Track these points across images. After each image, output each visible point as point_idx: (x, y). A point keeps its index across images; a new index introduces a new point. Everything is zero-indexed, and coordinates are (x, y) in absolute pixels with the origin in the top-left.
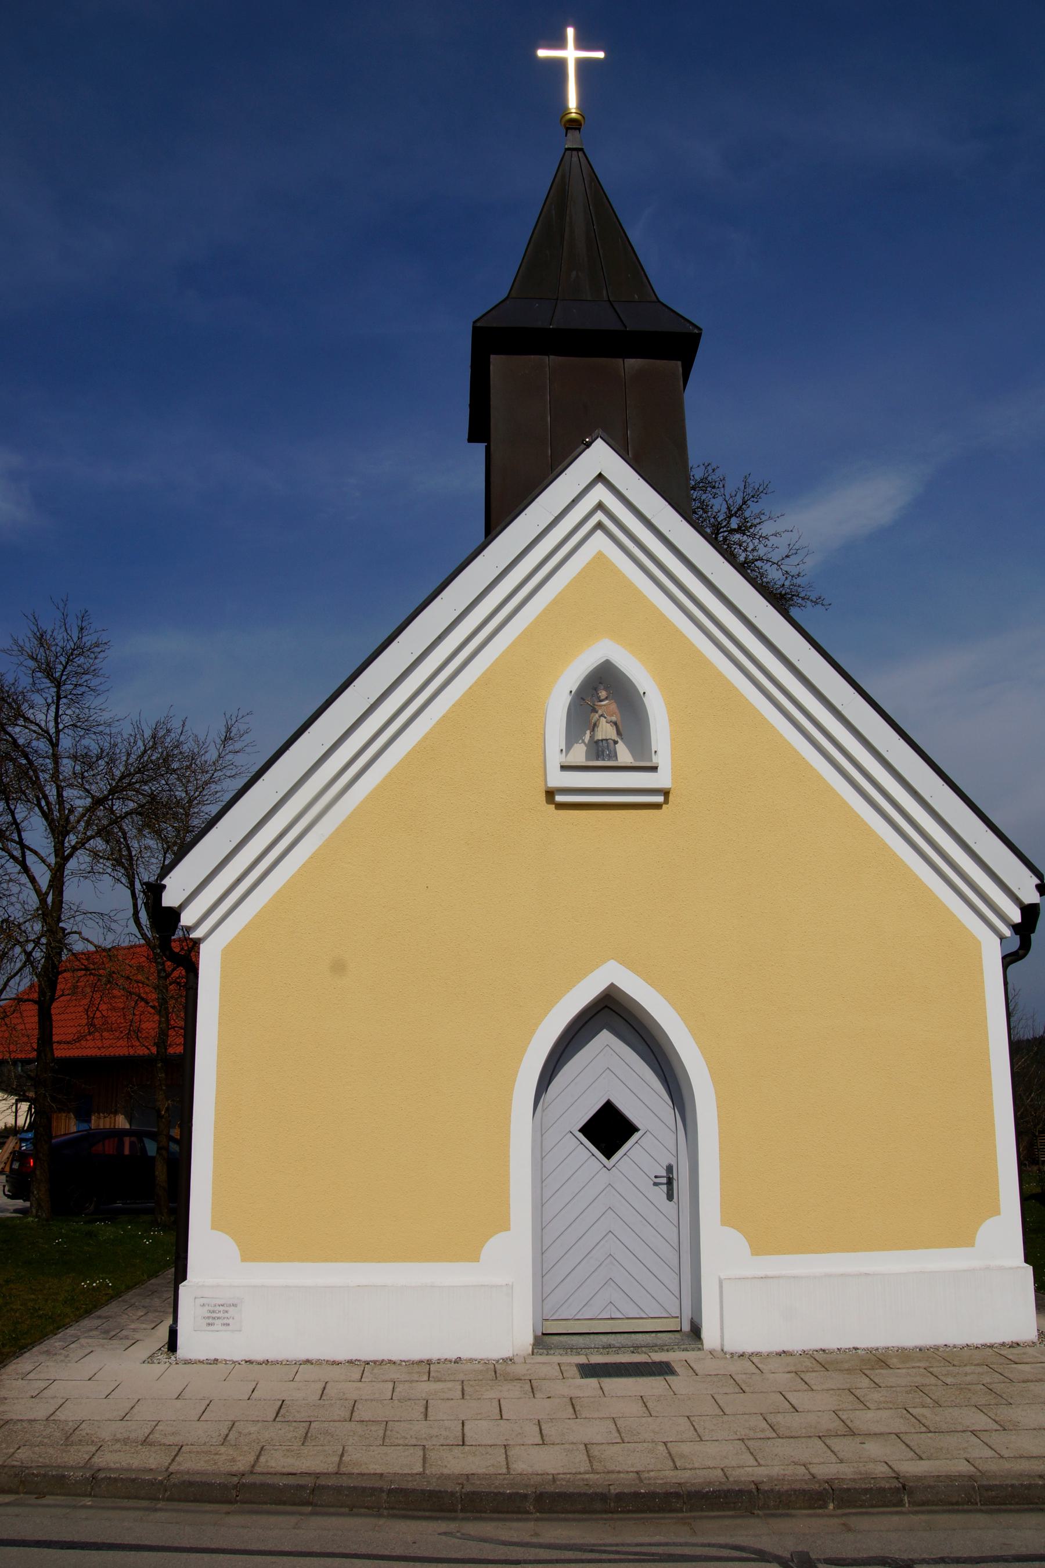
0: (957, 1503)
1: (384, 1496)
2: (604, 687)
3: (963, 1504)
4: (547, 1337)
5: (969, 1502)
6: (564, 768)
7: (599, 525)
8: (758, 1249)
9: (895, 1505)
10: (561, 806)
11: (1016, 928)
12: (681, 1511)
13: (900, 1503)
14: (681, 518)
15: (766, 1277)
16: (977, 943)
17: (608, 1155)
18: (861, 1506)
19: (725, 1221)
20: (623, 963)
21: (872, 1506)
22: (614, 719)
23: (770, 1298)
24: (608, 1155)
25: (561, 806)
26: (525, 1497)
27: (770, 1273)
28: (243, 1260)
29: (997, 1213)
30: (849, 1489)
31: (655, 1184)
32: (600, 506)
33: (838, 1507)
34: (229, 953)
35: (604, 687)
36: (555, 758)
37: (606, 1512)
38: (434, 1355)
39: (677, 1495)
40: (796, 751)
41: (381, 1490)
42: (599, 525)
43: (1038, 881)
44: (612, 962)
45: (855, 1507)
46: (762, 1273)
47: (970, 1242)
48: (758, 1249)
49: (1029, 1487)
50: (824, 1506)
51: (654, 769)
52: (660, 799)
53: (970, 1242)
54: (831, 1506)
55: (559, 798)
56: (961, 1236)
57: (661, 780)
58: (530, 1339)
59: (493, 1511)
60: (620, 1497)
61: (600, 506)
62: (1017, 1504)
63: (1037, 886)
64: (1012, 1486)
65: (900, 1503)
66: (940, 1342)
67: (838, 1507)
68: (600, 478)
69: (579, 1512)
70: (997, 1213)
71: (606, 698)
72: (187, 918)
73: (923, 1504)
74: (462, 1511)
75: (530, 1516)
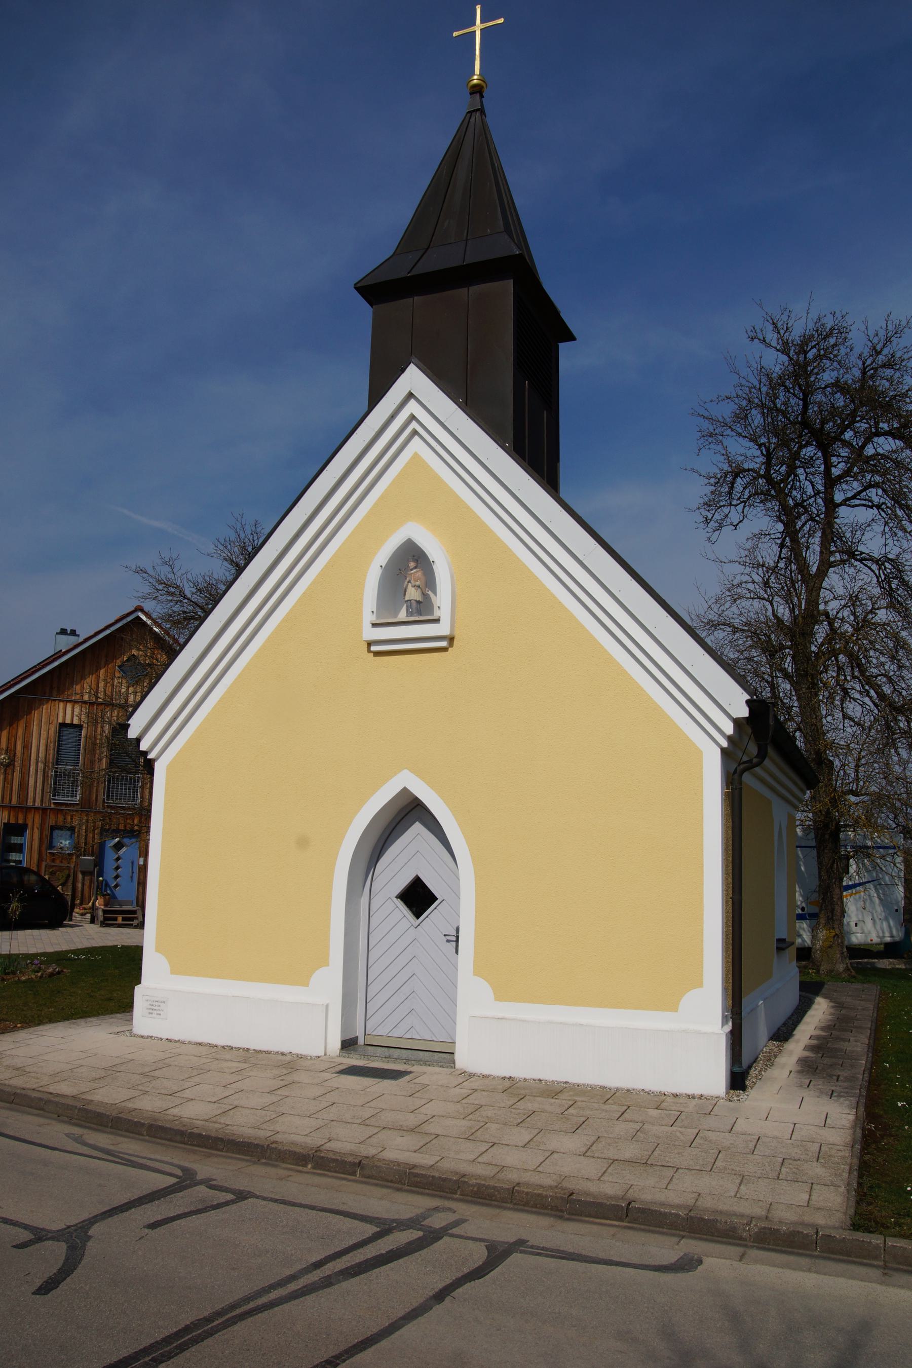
0: (391, 1181)
1: (76, 1111)
2: (411, 560)
3: (395, 1183)
4: (369, 1048)
5: (400, 1182)
6: (374, 625)
7: (415, 433)
8: (499, 997)
9: (350, 1174)
10: (377, 654)
11: (729, 738)
12: (221, 1150)
13: (354, 1174)
14: (467, 417)
15: (503, 1019)
16: (699, 753)
17: (418, 915)
18: (328, 1170)
19: (158, 950)
20: (412, 771)
21: (335, 1172)
22: (418, 583)
23: (504, 1034)
24: (418, 915)
25: (377, 654)
26: (143, 1124)
27: (507, 1016)
28: (172, 973)
29: (700, 985)
30: (323, 1157)
31: (448, 941)
32: (413, 418)
33: (314, 1168)
34: (170, 767)
35: (411, 560)
36: (368, 617)
37: (181, 1142)
38: (253, 1046)
39: (221, 1140)
40: (554, 596)
41: (76, 1107)
42: (415, 433)
43: (748, 697)
44: (406, 771)
45: (324, 1170)
46: (500, 1015)
47: (674, 1008)
48: (499, 997)
49: (445, 1180)
50: (305, 1166)
51: (437, 621)
52: (444, 644)
53: (674, 1008)
54: (310, 1166)
55: (373, 648)
56: (668, 1002)
57: (443, 629)
58: (339, 1045)
59: (127, 1131)
60: (192, 1135)
61: (413, 418)
62: (433, 1190)
63: (747, 702)
64: (433, 1177)
65: (354, 1174)
66: (639, 1086)
67: (314, 1168)
68: (411, 395)
69: (168, 1140)
70: (700, 985)
71: (415, 568)
72: (143, 746)
73: (369, 1177)
74: (111, 1127)
75: (141, 1137)
